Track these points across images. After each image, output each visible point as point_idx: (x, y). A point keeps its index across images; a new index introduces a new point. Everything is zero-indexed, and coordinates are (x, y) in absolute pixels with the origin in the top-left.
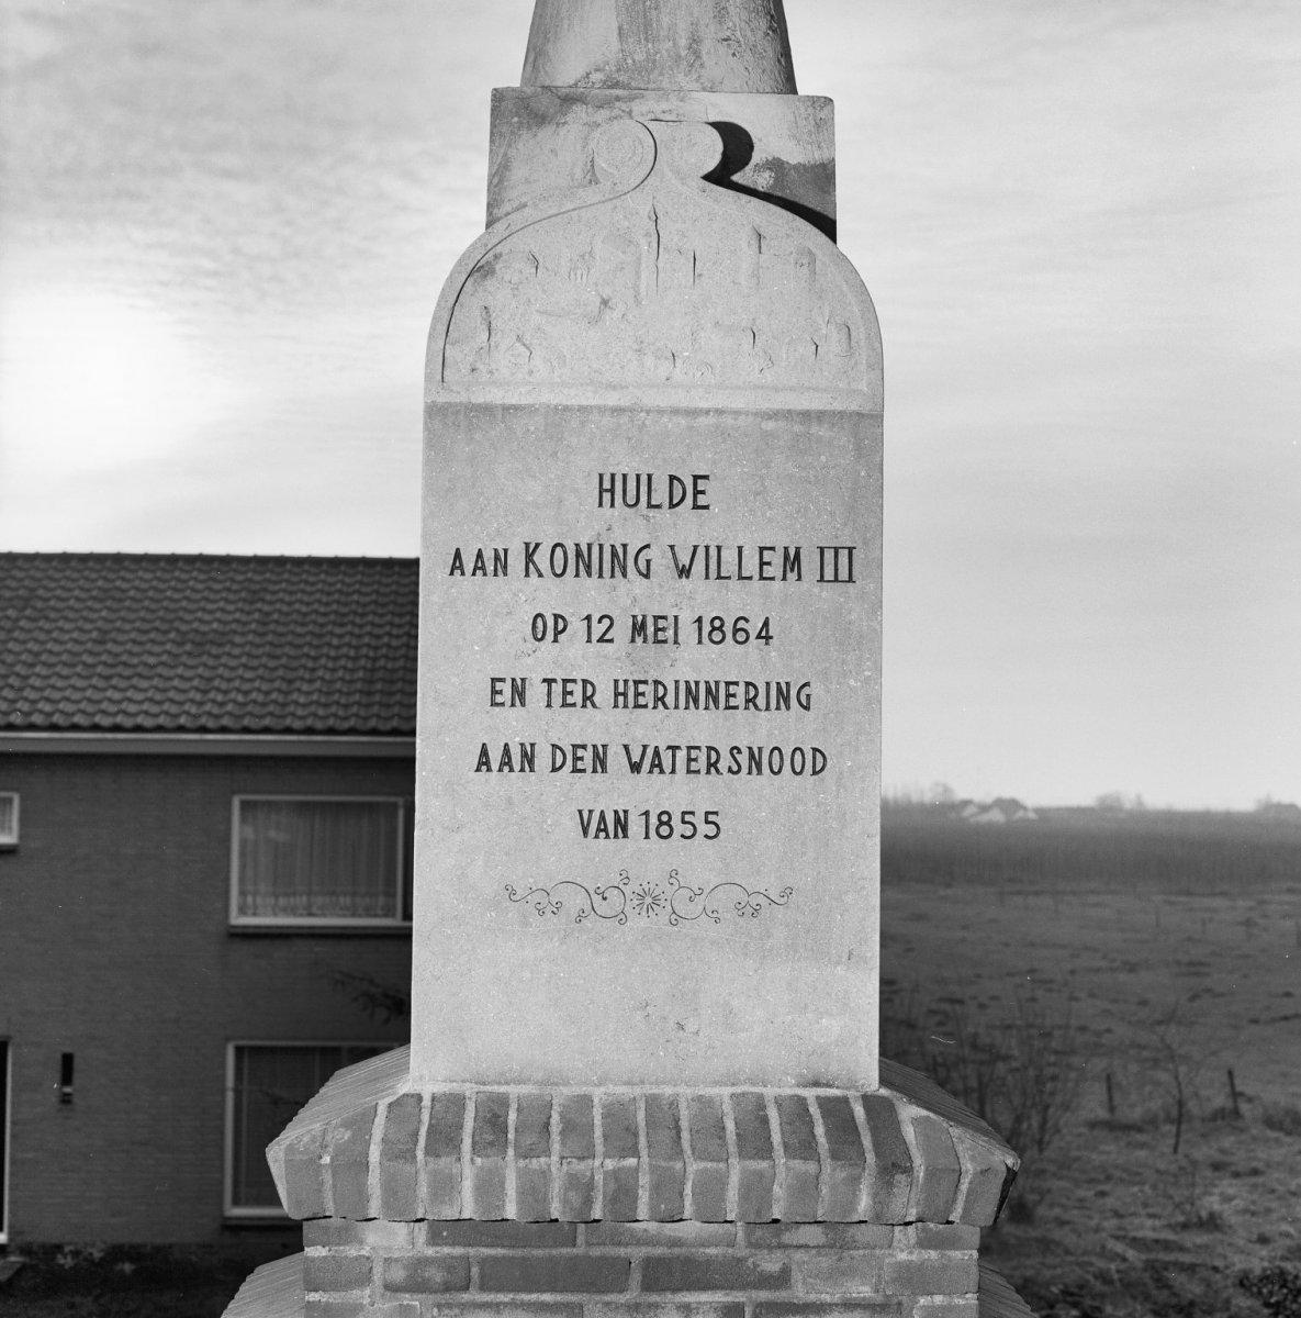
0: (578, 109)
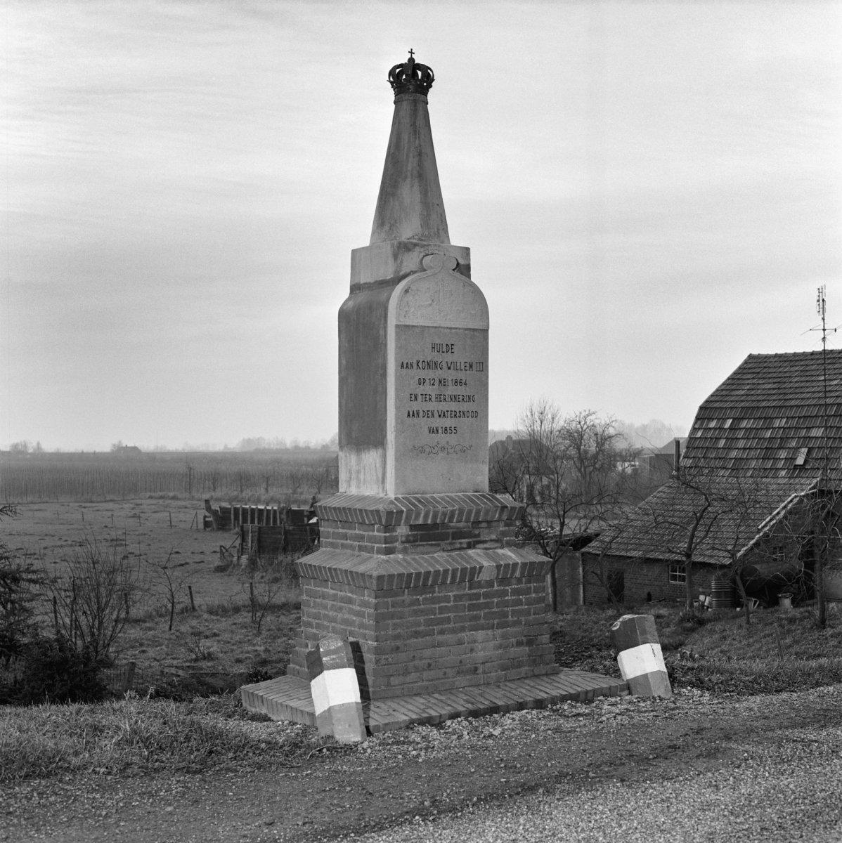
0: (417, 247)
